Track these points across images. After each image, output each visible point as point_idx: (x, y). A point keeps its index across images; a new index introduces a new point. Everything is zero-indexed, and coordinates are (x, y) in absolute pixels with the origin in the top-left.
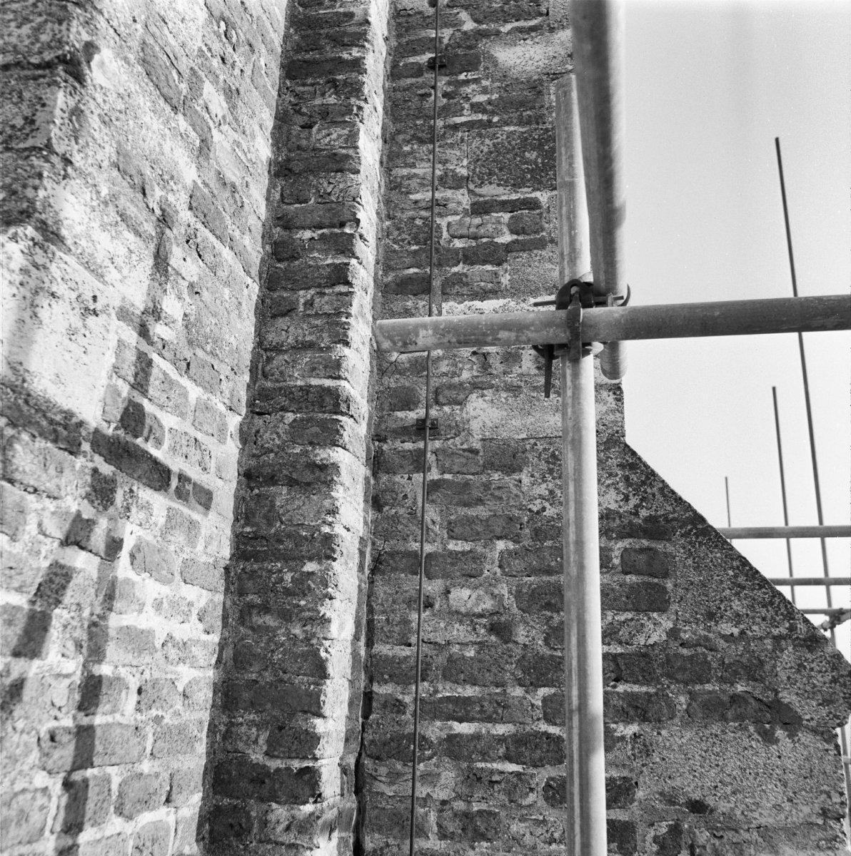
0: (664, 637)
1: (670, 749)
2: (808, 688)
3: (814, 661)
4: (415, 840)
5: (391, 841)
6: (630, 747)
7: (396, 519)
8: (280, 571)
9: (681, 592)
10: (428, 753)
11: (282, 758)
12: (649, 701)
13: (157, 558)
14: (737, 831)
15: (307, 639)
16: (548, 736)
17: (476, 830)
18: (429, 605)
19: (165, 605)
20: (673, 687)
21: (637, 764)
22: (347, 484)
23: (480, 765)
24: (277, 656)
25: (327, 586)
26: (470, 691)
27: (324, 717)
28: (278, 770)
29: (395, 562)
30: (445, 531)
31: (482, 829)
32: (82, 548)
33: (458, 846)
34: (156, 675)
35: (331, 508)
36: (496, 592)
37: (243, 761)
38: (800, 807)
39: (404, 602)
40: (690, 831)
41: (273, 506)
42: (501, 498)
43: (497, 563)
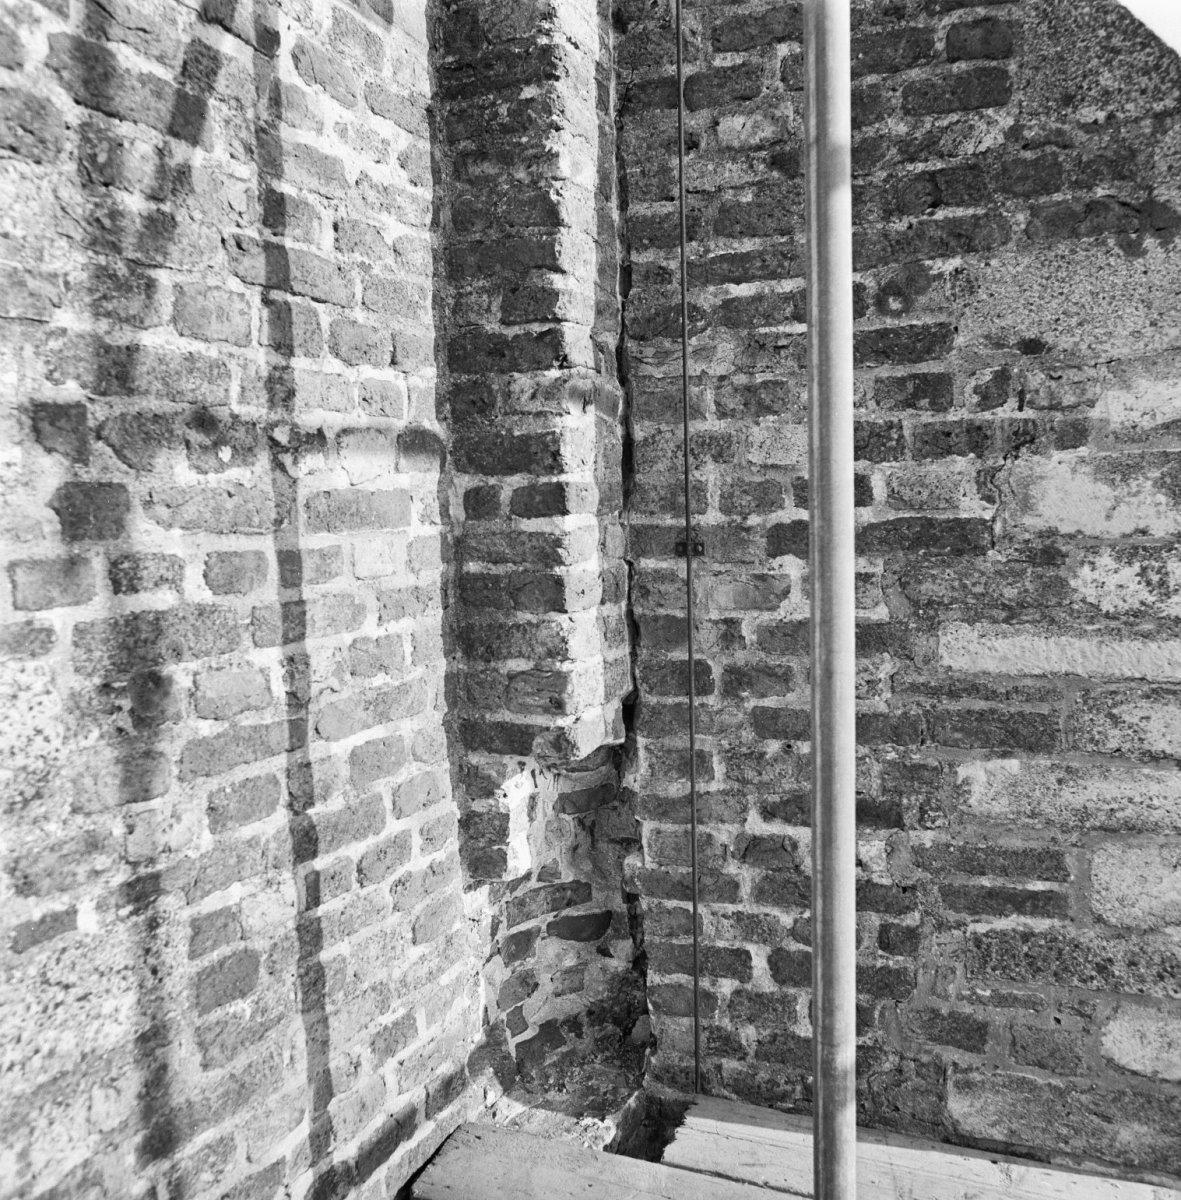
0: (1001, 139)
1: (1001, 281)
4: (690, 424)
5: (663, 427)
6: (949, 285)
7: (644, 37)
8: (493, 104)
9: (1028, 73)
10: (700, 324)
11: (519, 323)
14: (1079, 368)
15: (534, 183)
17: (760, 403)
18: (693, 145)
19: (351, 132)
20: (1008, 203)
21: (957, 305)
23: (763, 330)
24: (502, 208)
25: (550, 113)
26: (748, 245)
27: (563, 272)
28: (516, 337)
29: (648, 96)
30: (709, 44)
31: (768, 402)
32: (228, 30)
33: (740, 424)
34: (354, 216)
35: (546, 10)
36: (778, 113)
37: (476, 332)
39: (661, 145)
41: (475, 21)
43: (779, 75)
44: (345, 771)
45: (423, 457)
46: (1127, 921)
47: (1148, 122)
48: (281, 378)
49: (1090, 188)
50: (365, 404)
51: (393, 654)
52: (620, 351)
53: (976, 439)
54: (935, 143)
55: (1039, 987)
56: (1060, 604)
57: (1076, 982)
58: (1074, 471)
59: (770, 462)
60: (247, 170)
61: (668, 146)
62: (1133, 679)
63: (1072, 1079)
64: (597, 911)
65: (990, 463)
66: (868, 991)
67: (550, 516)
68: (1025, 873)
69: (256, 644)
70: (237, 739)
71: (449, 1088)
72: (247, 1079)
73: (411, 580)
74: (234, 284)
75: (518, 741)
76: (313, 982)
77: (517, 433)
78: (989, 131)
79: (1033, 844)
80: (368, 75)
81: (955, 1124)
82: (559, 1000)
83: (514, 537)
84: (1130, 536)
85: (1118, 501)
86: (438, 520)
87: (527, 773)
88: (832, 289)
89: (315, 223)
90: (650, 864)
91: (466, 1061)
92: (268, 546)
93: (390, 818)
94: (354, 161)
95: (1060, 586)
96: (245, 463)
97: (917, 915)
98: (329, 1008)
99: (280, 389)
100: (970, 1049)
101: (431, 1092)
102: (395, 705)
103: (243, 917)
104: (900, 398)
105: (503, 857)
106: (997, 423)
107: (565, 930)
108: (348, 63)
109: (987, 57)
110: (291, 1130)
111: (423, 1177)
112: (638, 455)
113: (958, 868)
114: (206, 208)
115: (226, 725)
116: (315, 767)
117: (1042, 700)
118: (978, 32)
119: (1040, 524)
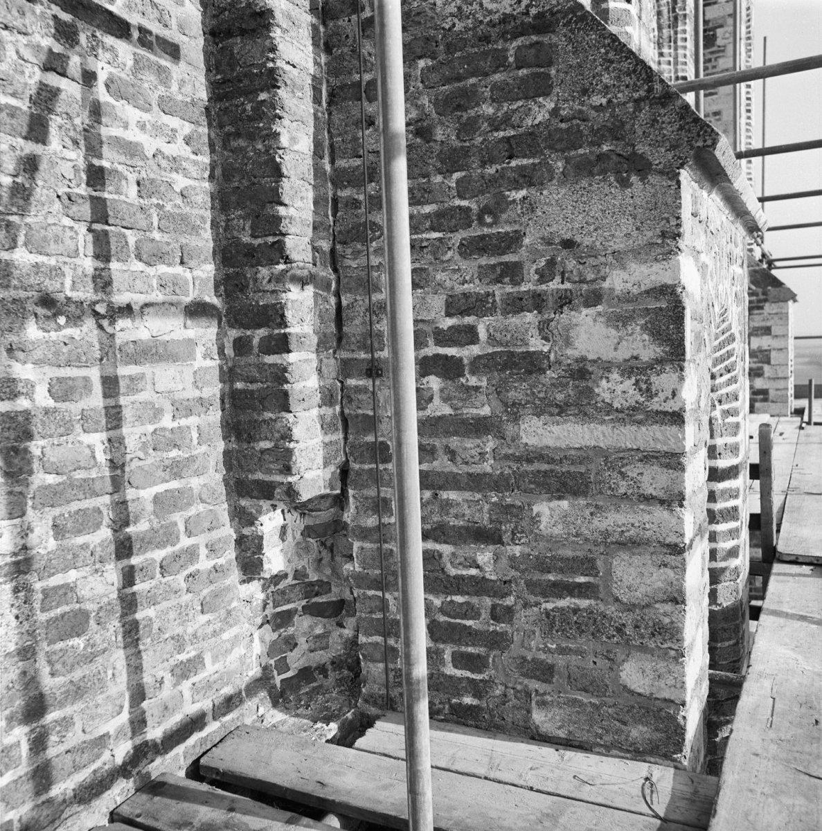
2: (659, 138)
3: (666, 115)
5: (358, 298)
6: (519, 207)
7: (341, 57)
8: (243, 104)
11: (261, 237)
12: (534, 170)
13: (131, 90)
14: (596, 257)
15: (267, 151)
16: (460, 207)
19: (148, 126)
21: (524, 219)
22: (284, 26)
25: (275, 109)
27: (286, 205)
28: (260, 245)
34: (152, 176)
36: (419, 103)
37: (237, 242)
38: (645, 232)
40: (562, 262)
41: (232, 54)
42: (420, 23)
44: (150, 507)
45: (204, 319)
46: (633, 600)
47: (631, 105)
48: (100, 275)
49: (599, 146)
50: (162, 289)
51: (183, 438)
52: (333, 251)
53: (537, 302)
54: (510, 119)
55: (583, 642)
56: (589, 404)
57: (604, 639)
58: (595, 321)
59: (419, 318)
60: (77, 156)
61: (358, 124)
62: (632, 450)
63: (604, 699)
64: (334, 599)
65: (546, 316)
66: (485, 646)
67: (281, 353)
68: (574, 572)
69: (85, 431)
70: (72, 486)
71: (230, 703)
72: (82, 684)
73: (197, 394)
74: (67, 222)
75: (266, 491)
76: (132, 633)
77: (261, 304)
78: (540, 112)
79: (579, 553)
80: (161, 90)
81: (537, 727)
82: (312, 654)
83: (261, 367)
84: (628, 360)
85: (621, 339)
86: (216, 357)
87: (279, 511)
88: (394, 218)
89: (124, 182)
90: (358, 569)
91: (243, 687)
92: (94, 374)
93: (183, 537)
94: (150, 144)
95: (588, 393)
96: (76, 325)
97: (512, 598)
98: (141, 647)
99: (103, 282)
100: (545, 681)
101: (217, 703)
102: (185, 469)
103: (78, 590)
104: (493, 277)
105: (261, 562)
106: (549, 292)
107: (310, 610)
108: (146, 85)
109: (538, 66)
110: (113, 717)
111: (208, 754)
112: (344, 315)
113: (535, 568)
114: (46, 178)
115: (65, 478)
116: (129, 504)
117: (580, 463)
118: (533, 51)
119: (576, 354)
